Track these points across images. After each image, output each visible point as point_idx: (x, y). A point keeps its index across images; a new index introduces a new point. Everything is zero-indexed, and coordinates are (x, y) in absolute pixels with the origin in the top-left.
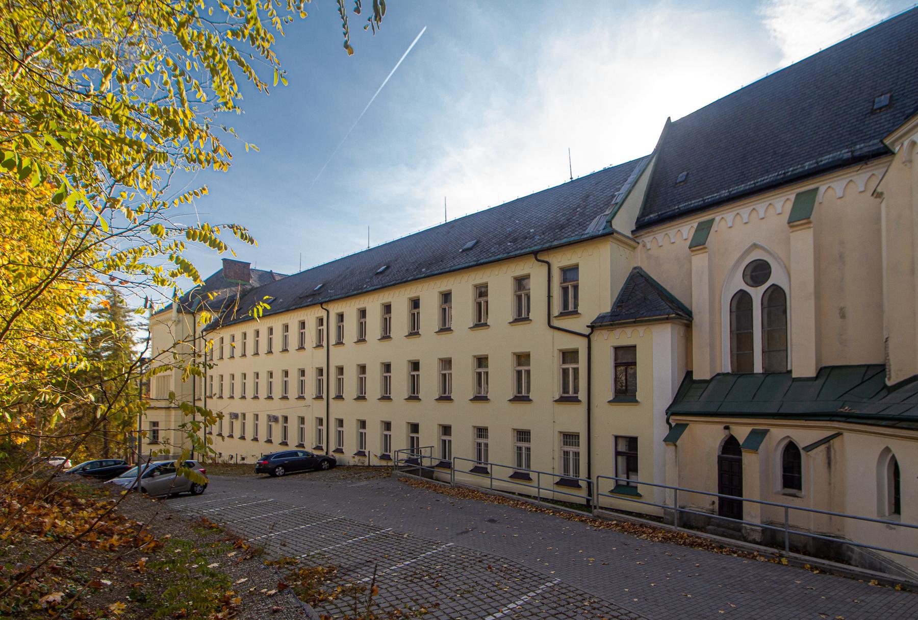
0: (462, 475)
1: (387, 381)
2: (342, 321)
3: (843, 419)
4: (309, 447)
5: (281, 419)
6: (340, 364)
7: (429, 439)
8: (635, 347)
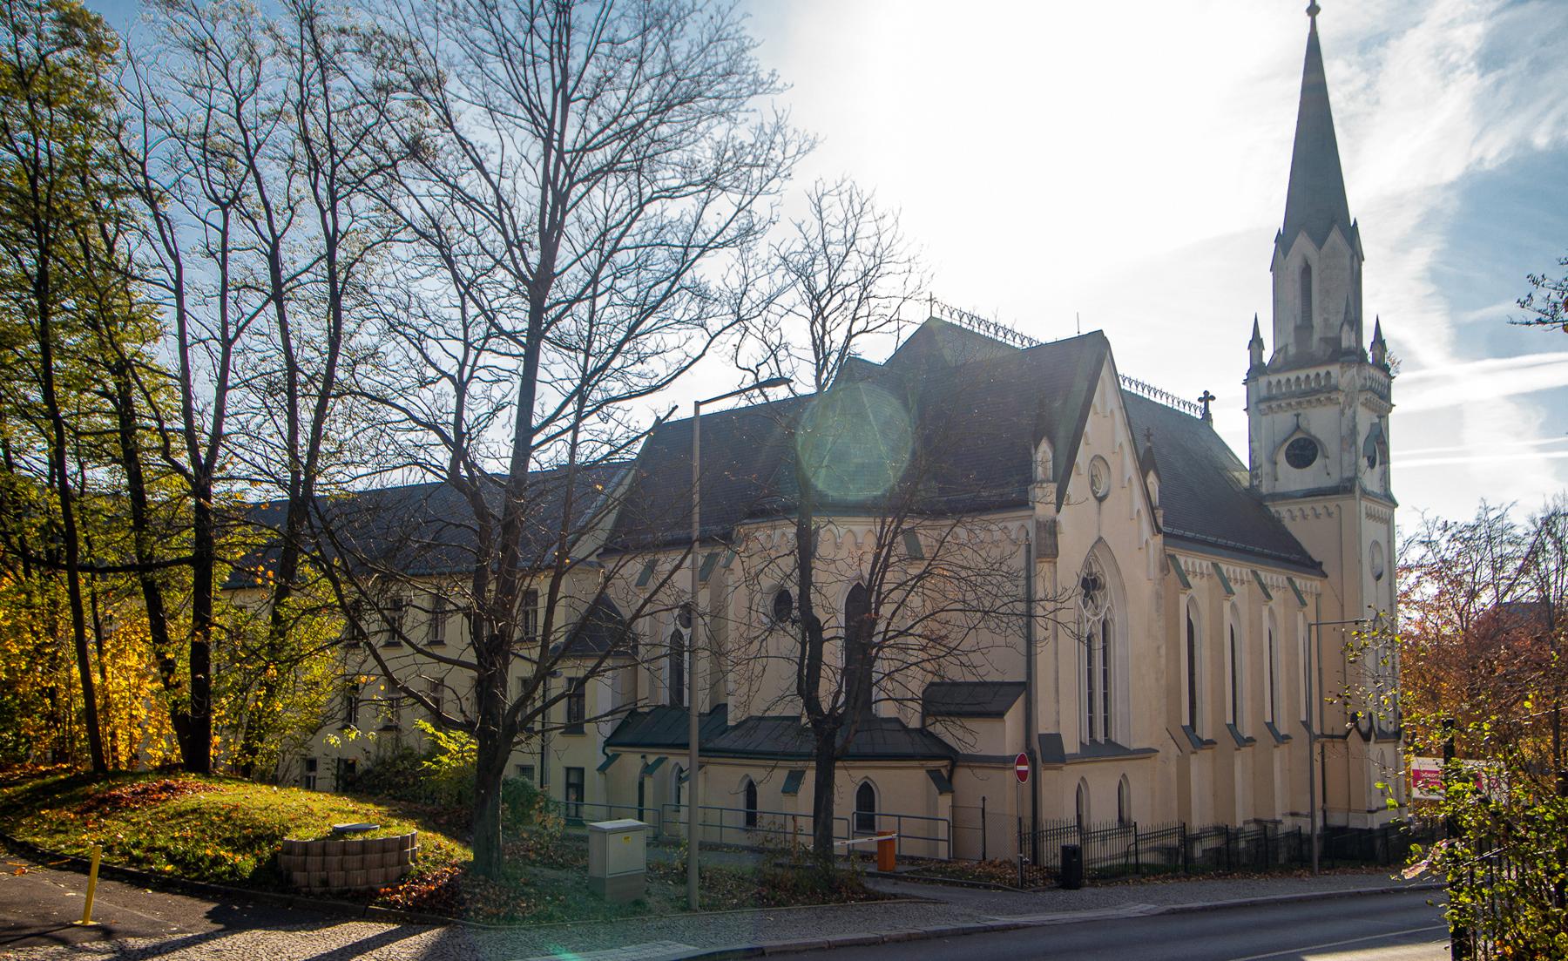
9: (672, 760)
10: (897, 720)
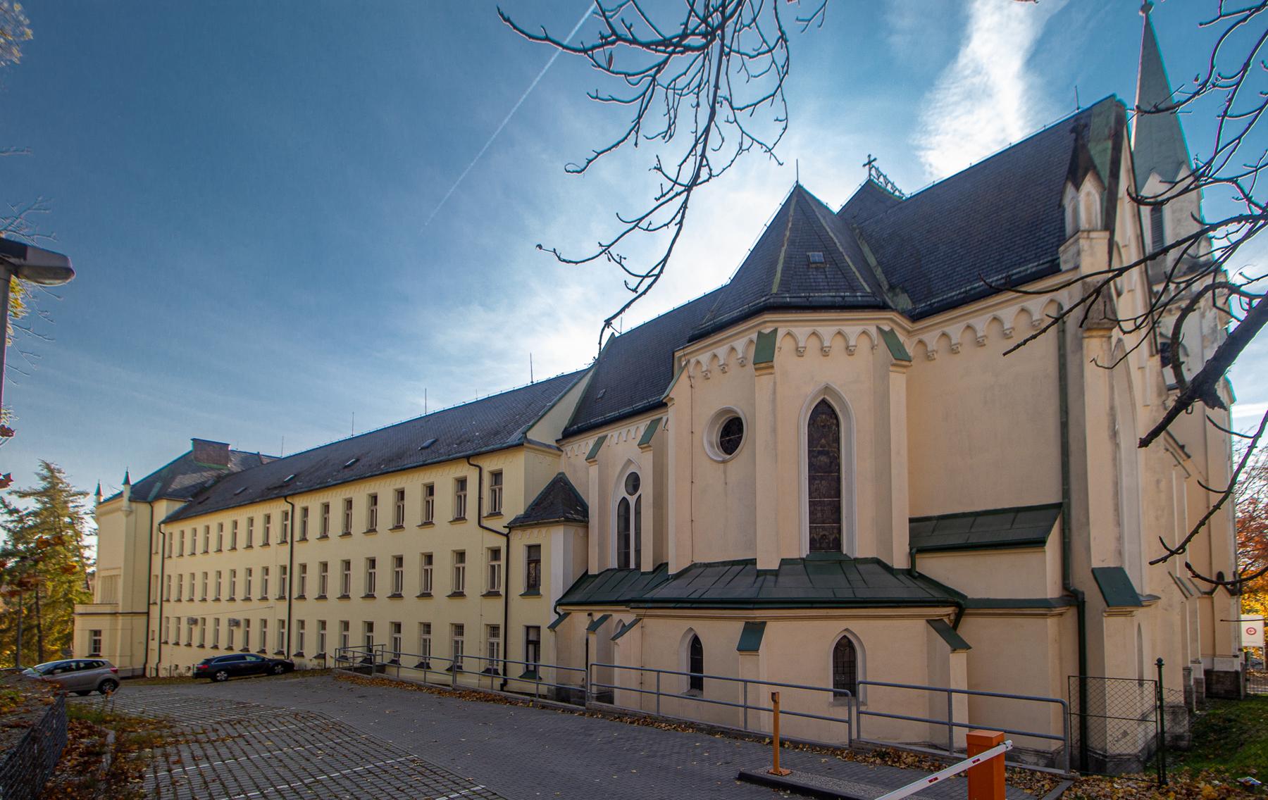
0: (408, 672)
1: (427, 575)
2: (402, 499)
3: (623, 608)
4: (270, 655)
5: (243, 624)
6: (302, 562)
7: (382, 637)
8: (539, 546)
9: (616, 617)
10: (877, 561)
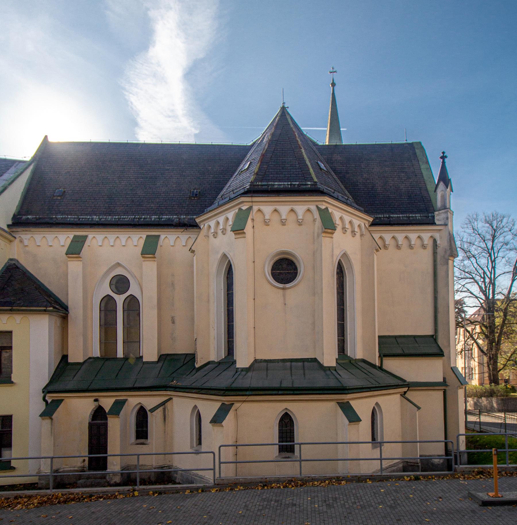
8: (11, 332)
